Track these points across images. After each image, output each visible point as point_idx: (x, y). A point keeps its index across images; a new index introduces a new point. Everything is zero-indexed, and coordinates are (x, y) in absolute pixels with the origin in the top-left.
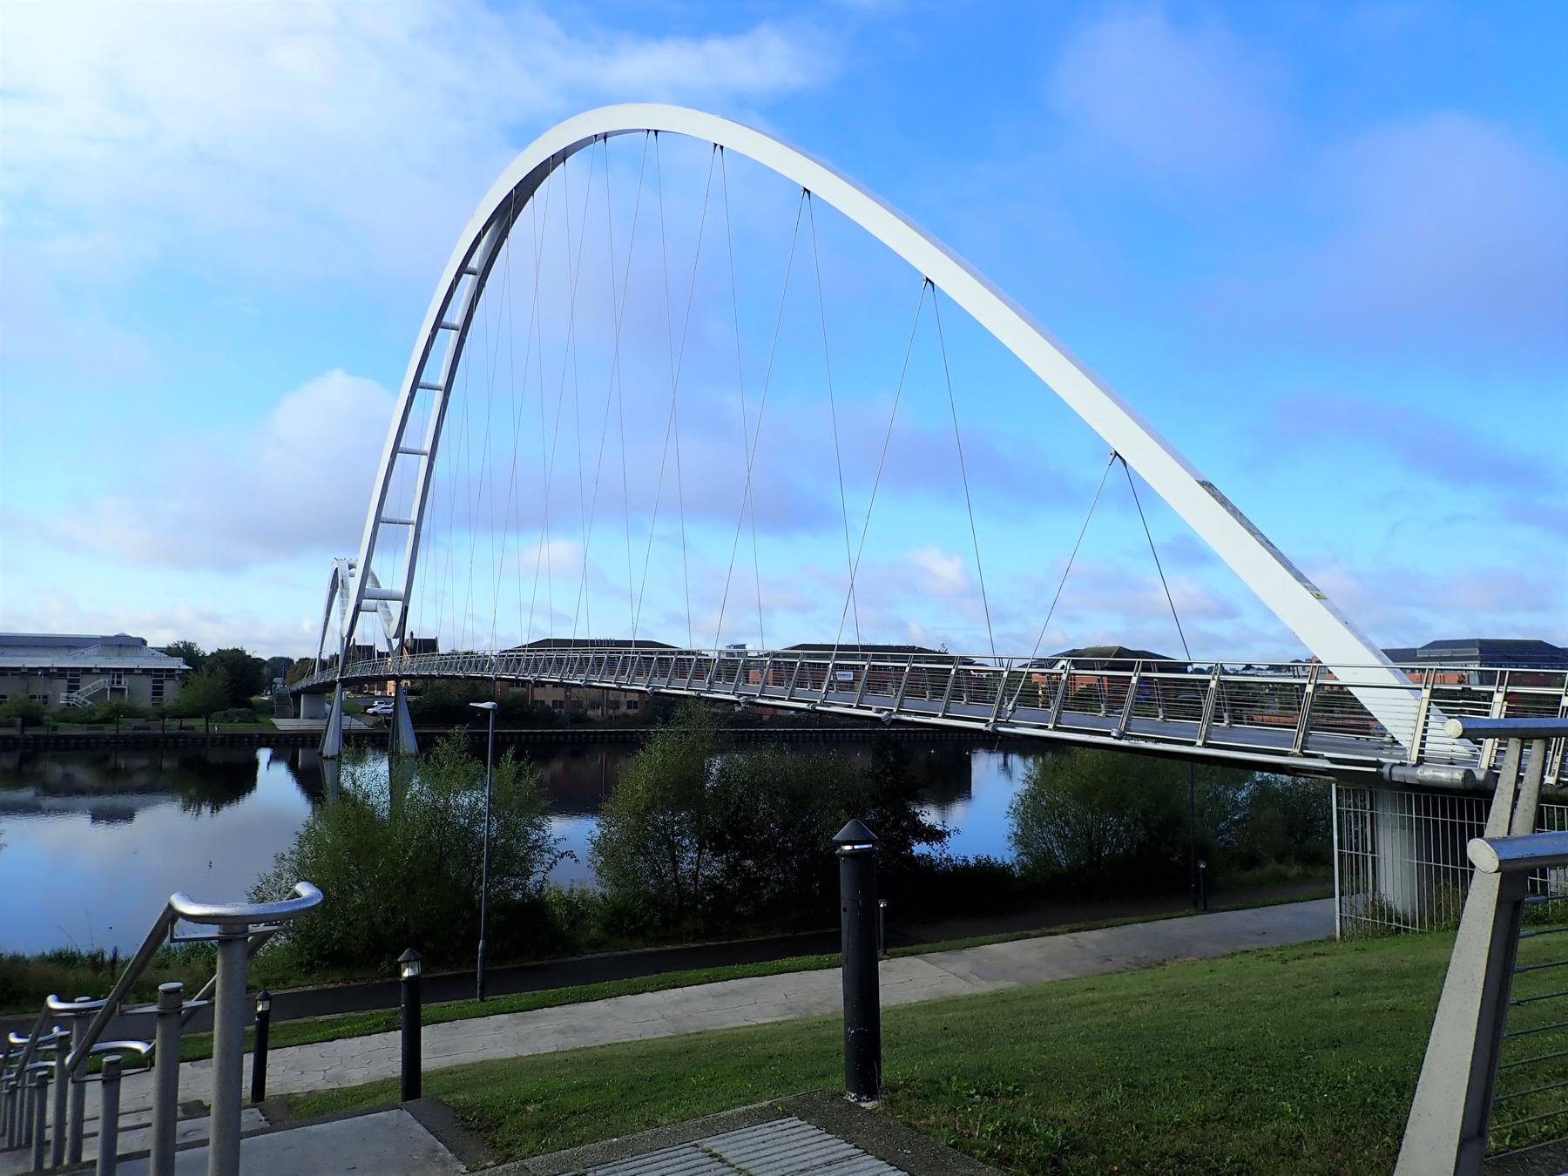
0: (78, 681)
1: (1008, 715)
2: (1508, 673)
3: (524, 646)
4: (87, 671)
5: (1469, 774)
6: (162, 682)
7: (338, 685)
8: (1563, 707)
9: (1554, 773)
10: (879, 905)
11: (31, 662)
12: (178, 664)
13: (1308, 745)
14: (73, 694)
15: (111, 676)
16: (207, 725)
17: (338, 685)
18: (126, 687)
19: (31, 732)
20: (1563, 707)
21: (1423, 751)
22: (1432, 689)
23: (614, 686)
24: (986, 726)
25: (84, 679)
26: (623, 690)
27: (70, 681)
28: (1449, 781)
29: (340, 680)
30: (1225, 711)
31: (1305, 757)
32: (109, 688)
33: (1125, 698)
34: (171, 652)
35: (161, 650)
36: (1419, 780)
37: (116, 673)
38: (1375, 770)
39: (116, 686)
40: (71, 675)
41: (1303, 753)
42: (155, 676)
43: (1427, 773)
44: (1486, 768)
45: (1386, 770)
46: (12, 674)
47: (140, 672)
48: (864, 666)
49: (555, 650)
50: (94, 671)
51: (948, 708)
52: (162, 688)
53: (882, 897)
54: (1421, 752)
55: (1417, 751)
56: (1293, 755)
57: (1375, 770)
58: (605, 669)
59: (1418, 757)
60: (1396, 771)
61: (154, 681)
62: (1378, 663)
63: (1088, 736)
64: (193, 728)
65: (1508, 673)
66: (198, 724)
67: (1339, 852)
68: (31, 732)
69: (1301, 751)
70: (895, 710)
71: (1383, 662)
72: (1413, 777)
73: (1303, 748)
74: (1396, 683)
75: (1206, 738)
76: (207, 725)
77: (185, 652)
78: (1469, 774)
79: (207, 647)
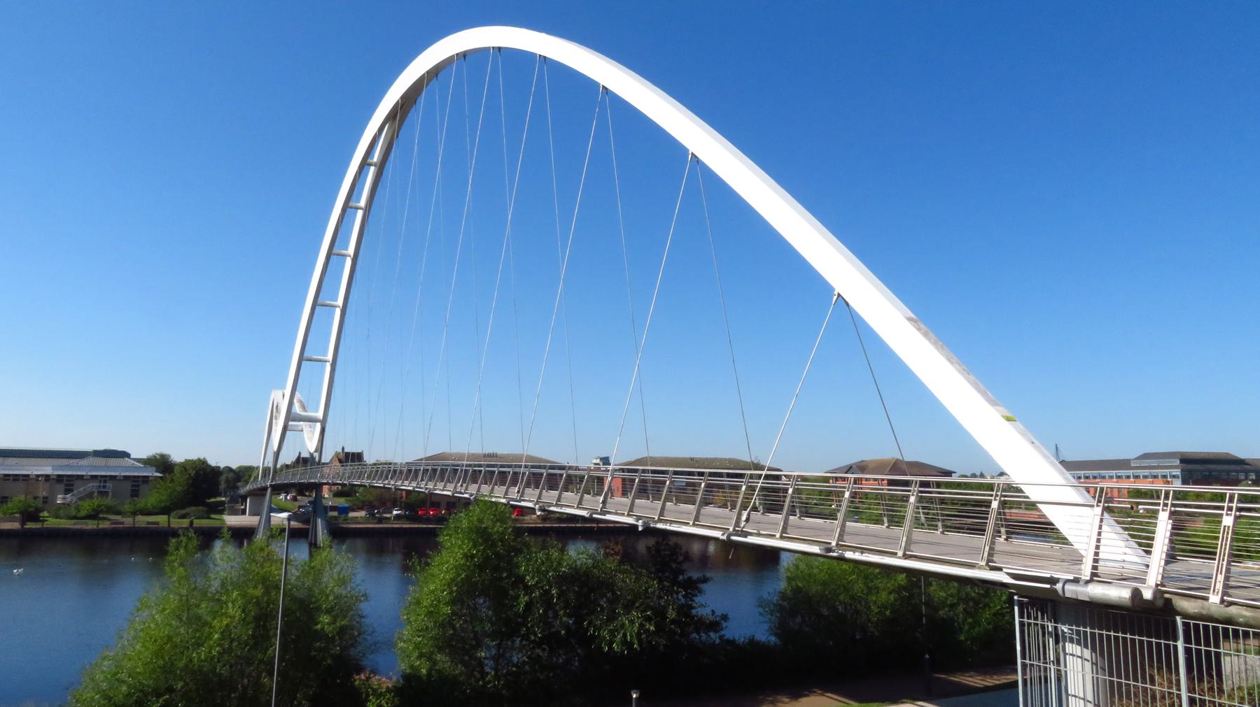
0: (72, 485)
1: (742, 526)
2: (1172, 492)
3: (422, 459)
4: (80, 477)
5: (1136, 593)
6: (138, 486)
7: (269, 490)
8: (1225, 526)
9: (1218, 592)
10: (632, 697)
11: (36, 470)
12: (152, 473)
13: (994, 559)
14: (67, 496)
15: (98, 481)
16: (169, 522)
17: (269, 490)
18: (110, 490)
19: (30, 525)
20: (1225, 526)
21: (1097, 566)
22: (1235, 516)
23: (381, 485)
24: (723, 535)
25: (78, 483)
26: (387, 488)
27: (66, 485)
28: (1118, 599)
29: (271, 485)
30: (1002, 526)
31: (991, 570)
32: (96, 491)
33: (986, 523)
34: (148, 462)
35: (139, 460)
36: (1090, 597)
37: (102, 479)
38: (1048, 586)
39: (101, 490)
40: (67, 481)
41: (989, 566)
42: (134, 481)
43: (1097, 591)
44: (1154, 585)
45: (1059, 586)
46: (23, 480)
47: (89, 478)
48: (562, 475)
49: (731, 493)
50: (118, 478)
51: (632, 509)
52: (138, 491)
53: (636, 688)
54: (1095, 568)
55: (1091, 567)
56: (980, 568)
57: (1048, 586)
58: (543, 486)
59: (1092, 573)
60: (1069, 587)
61: (133, 486)
62: (1063, 482)
63: (806, 546)
64: (157, 523)
65: (1172, 492)
66: (162, 520)
67: (1022, 663)
68: (30, 525)
69: (987, 564)
70: (656, 519)
71: (1066, 479)
72: (1082, 593)
73: (988, 561)
74: (1080, 501)
75: (906, 550)
76: (169, 522)
77: (162, 464)
78: (1136, 593)
79: (178, 457)
